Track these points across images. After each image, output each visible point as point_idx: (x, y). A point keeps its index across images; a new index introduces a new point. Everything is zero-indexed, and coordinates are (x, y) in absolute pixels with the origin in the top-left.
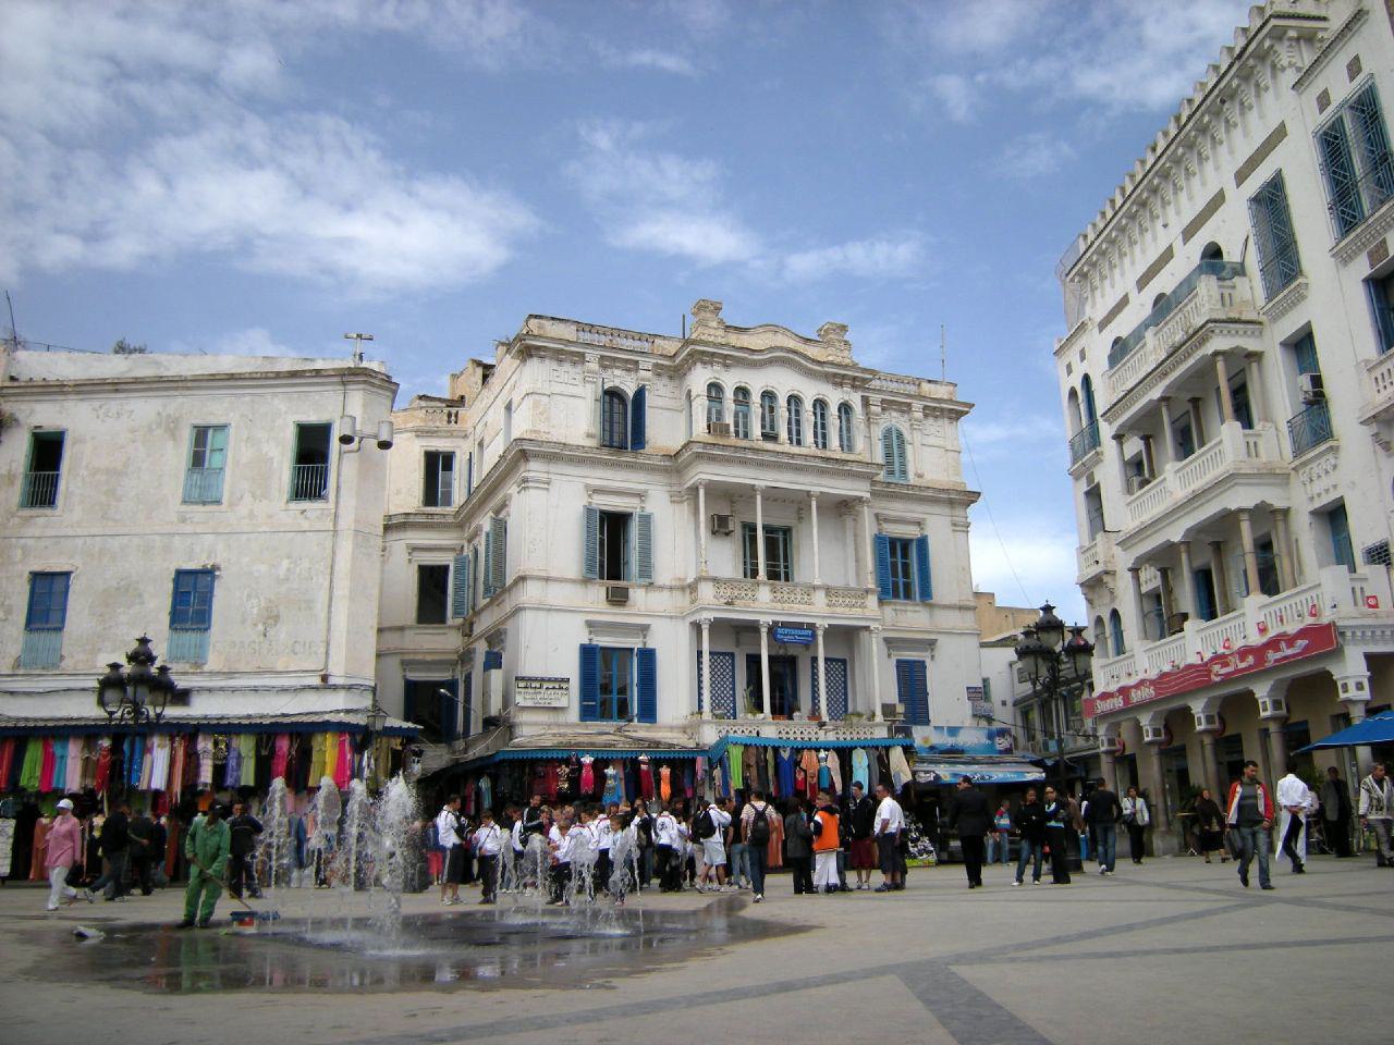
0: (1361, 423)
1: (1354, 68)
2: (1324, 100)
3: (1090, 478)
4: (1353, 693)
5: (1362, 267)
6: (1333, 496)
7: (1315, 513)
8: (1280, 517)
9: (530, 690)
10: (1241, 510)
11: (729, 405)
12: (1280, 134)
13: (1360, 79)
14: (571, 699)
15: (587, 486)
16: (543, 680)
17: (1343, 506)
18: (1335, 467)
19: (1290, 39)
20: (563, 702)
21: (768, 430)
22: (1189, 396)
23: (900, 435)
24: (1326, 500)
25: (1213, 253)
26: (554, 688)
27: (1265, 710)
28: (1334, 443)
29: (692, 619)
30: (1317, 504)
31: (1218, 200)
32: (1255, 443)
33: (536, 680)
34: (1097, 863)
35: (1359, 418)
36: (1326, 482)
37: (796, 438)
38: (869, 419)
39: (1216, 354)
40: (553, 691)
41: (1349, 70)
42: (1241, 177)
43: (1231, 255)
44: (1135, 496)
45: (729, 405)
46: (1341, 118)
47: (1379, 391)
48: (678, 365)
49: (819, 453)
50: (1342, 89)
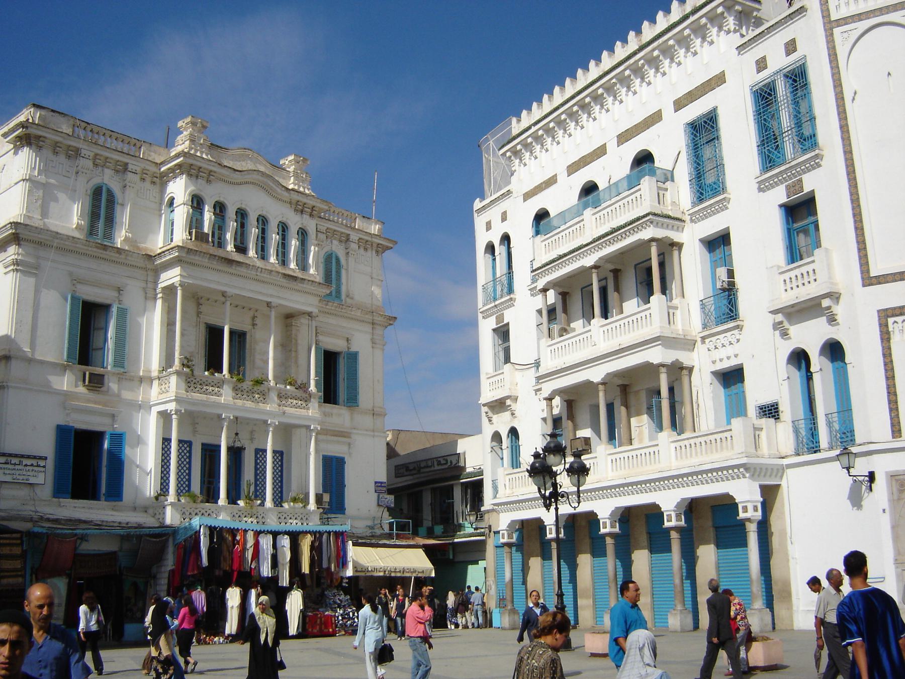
0: (770, 312)
1: (791, 47)
2: (761, 64)
3: (500, 319)
4: (750, 514)
5: (780, 195)
6: (733, 362)
7: (715, 374)
8: (685, 372)
9: (9, 466)
10: (663, 365)
11: (208, 216)
12: (719, 80)
13: (794, 57)
14: (44, 478)
15: (71, 274)
16: (22, 456)
17: (742, 369)
18: (738, 341)
19: (736, 11)
20: (40, 479)
21: (239, 243)
22: (613, 267)
23: (110, 194)
24: (726, 365)
25: (644, 159)
26: (32, 465)
27: (669, 520)
28: (739, 323)
29: (162, 408)
30: (720, 366)
31: (655, 118)
32: (674, 313)
33: (16, 456)
34: (397, 636)
35: (768, 308)
36: (730, 351)
37: (263, 256)
38: (348, 253)
39: (653, 240)
40: (31, 468)
41: (786, 47)
42: (679, 105)
43: (662, 161)
44: (554, 341)
45: (208, 216)
46: (774, 82)
47: (786, 290)
48: (163, 172)
49: (280, 269)
50: (778, 61)
